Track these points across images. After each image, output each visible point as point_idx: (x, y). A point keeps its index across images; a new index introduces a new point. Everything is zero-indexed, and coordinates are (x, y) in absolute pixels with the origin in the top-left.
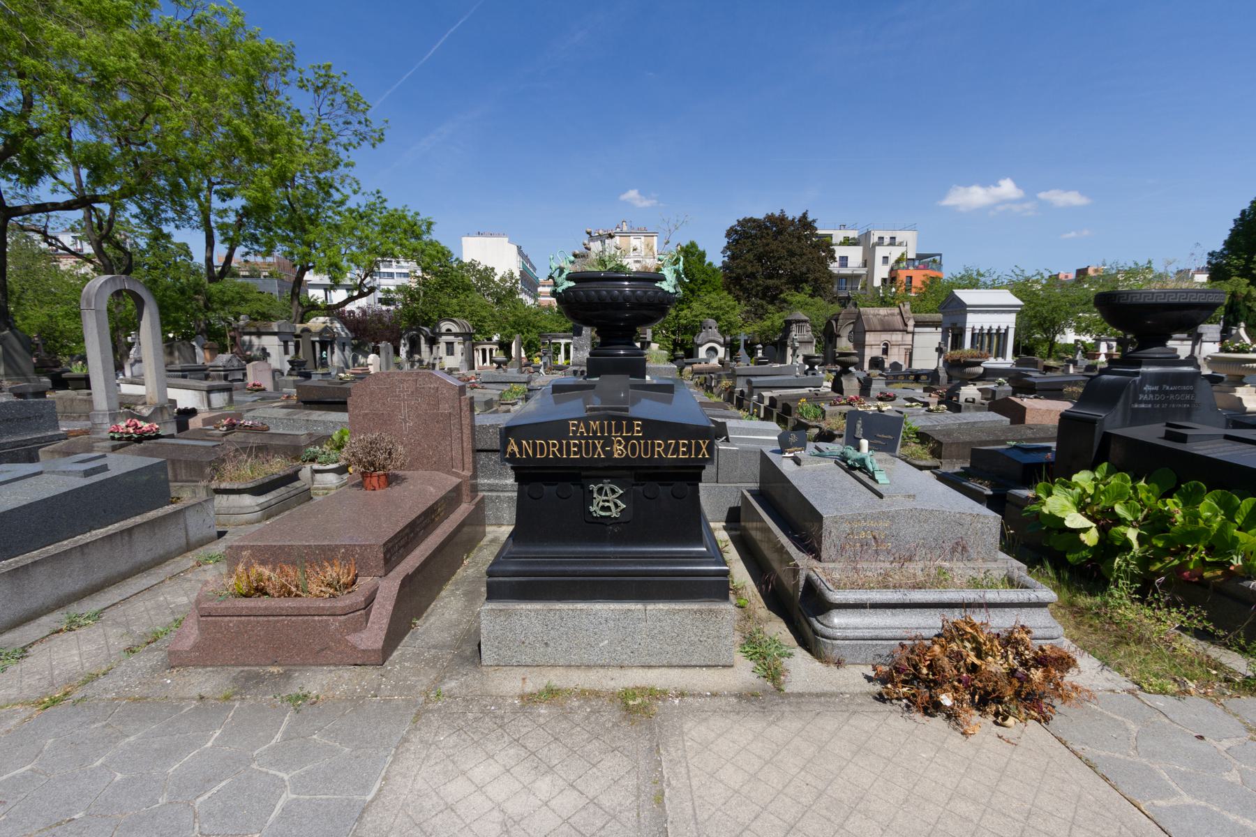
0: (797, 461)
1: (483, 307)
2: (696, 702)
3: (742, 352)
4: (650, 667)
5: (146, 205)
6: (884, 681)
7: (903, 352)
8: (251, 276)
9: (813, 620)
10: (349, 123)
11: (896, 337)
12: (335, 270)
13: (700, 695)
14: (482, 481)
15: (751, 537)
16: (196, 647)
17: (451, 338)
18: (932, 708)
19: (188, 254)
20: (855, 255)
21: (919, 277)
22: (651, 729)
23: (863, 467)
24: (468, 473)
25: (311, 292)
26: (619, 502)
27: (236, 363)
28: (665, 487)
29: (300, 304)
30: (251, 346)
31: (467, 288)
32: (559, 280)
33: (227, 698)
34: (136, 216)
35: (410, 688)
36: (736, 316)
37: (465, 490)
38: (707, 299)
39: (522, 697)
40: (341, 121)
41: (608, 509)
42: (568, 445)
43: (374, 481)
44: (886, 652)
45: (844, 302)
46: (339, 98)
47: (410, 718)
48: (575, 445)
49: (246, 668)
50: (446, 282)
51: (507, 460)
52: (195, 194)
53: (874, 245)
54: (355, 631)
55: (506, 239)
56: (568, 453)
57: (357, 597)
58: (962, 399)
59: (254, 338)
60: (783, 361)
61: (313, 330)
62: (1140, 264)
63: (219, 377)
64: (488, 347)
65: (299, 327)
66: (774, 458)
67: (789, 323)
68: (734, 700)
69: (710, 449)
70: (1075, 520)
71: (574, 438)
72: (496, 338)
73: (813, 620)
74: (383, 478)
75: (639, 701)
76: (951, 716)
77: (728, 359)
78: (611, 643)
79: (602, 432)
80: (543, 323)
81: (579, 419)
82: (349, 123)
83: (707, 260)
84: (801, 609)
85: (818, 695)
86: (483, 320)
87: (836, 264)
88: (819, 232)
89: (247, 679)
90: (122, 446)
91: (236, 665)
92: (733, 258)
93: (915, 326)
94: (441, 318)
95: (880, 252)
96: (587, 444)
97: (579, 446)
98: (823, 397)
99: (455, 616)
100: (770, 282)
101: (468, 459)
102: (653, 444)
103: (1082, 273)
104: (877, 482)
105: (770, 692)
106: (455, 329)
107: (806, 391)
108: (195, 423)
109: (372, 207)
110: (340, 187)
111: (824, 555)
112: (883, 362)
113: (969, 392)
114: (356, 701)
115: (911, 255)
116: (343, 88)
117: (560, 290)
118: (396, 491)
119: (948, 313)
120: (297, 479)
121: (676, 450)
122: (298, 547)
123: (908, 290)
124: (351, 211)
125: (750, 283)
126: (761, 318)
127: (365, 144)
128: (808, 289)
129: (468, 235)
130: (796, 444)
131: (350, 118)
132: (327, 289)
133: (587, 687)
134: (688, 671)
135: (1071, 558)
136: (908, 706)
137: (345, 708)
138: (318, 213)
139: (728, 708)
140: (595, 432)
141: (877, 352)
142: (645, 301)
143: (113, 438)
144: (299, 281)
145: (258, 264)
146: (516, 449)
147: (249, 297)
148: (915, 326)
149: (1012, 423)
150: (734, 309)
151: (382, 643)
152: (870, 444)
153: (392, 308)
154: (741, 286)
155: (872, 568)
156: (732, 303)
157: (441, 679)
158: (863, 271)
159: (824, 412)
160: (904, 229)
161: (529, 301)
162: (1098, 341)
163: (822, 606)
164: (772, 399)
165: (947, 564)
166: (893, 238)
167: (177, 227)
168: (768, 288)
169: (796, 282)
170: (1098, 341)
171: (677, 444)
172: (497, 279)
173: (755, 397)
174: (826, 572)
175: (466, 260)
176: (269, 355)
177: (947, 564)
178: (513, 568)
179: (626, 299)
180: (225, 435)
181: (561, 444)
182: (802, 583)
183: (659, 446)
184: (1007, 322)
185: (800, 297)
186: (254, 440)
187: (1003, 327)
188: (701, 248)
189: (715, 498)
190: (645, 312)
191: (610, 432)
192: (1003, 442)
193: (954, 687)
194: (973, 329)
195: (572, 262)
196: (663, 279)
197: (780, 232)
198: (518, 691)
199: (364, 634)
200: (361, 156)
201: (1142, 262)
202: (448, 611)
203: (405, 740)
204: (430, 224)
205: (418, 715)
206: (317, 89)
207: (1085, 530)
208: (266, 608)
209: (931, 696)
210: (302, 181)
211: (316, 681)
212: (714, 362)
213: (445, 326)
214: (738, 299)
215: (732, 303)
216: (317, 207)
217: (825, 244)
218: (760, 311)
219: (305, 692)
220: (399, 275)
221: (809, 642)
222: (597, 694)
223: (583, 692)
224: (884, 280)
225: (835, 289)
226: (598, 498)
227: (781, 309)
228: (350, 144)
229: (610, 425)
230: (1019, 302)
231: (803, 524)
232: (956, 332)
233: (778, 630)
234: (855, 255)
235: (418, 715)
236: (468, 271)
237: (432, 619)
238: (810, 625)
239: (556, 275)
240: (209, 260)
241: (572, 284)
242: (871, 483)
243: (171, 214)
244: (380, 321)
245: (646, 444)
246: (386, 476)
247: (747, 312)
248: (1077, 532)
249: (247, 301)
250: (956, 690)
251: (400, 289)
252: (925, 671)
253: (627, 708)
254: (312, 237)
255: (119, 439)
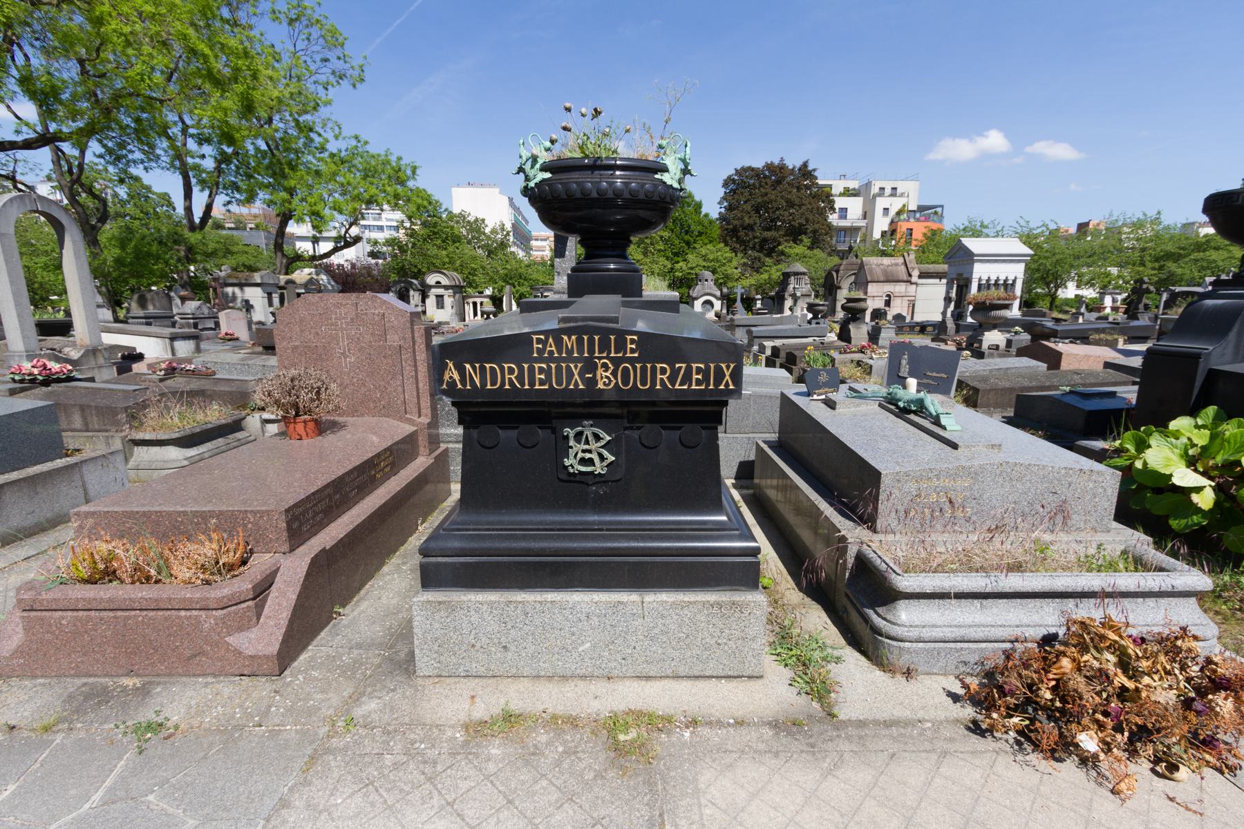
0: (831, 404)
1: (474, 258)
2: (714, 736)
3: (739, 304)
4: (648, 678)
5: (110, 144)
6: (975, 701)
7: (906, 304)
8: (236, 229)
9: (870, 612)
10: (326, 60)
11: (899, 288)
12: (318, 219)
13: (720, 724)
14: (442, 431)
15: (768, 499)
16: (19, 652)
17: (440, 291)
18: (1064, 748)
19: (170, 204)
20: (854, 207)
21: (919, 230)
22: (650, 784)
23: (921, 409)
24: (425, 420)
25: (298, 244)
26: (605, 453)
27: (206, 311)
28: (671, 429)
29: (284, 255)
30: (234, 298)
31: (457, 239)
32: (531, 173)
33: (46, 729)
34: (100, 156)
35: (311, 712)
36: (733, 269)
37: (422, 441)
38: (703, 251)
39: (466, 727)
40: (318, 58)
41: (590, 462)
42: (531, 369)
43: (300, 428)
44: (973, 658)
45: (843, 255)
46: (315, 32)
47: (300, 763)
48: (541, 370)
49: (91, 680)
50: (435, 233)
51: (444, 392)
52: (164, 132)
53: (875, 197)
54: (240, 629)
55: (497, 190)
56: (532, 384)
57: (243, 584)
58: (985, 346)
59: (237, 290)
60: (781, 311)
61: (298, 281)
62: (1149, 215)
63: (188, 325)
64: (478, 300)
65: (283, 278)
66: (801, 402)
67: (786, 276)
68: (768, 732)
69: (737, 376)
70: (1184, 477)
71: (540, 360)
72: (488, 292)
73: (870, 612)
74: (311, 425)
75: (633, 734)
76: (1087, 761)
77: (724, 311)
78: (594, 647)
79: (581, 351)
80: (535, 276)
81: (546, 333)
82: (326, 60)
83: (704, 210)
84: (857, 599)
85: (888, 724)
86: (473, 272)
87: (835, 216)
88: (820, 182)
89: (87, 697)
90: (23, 390)
91: (77, 676)
92: (730, 208)
93: (920, 277)
94: (431, 271)
95: (881, 203)
96: (559, 369)
97: (548, 372)
98: (831, 346)
99: (394, 601)
100: (768, 234)
101: (426, 402)
102: (654, 369)
103: (1082, 227)
104: (944, 428)
105: (816, 721)
106: (445, 281)
107: (810, 340)
108: (138, 367)
109: (354, 153)
110: (321, 132)
111: (880, 524)
112: (885, 313)
113: (993, 337)
114: (230, 733)
115: (913, 207)
116: (318, 21)
117: (532, 184)
118: (329, 440)
119: (954, 261)
120: (241, 429)
121: (687, 378)
122: (169, 514)
123: (908, 243)
124: (332, 155)
125: (747, 235)
126: (757, 271)
127: (344, 83)
128: (807, 240)
129: (458, 185)
130: (826, 385)
131: (328, 55)
132: (315, 240)
133: (560, 710)
134: (700, 684)
135: (1174, 524)
136: (1018, 743)
137: (211, 745)
138: (298, 158)
139: (762, 746)
140: (570, 352)
141: (879, 304)
142: (642, 196)
143: (13, 380)
144: (281, 232)
145: (242, 213)
146: (456, 376)
147: (235, 249)
148: (920, 277)
149: (1049, 369)
150: (730, 261)
151: (277, 646)
152: (919, 384)
153: (380, 261)
154: (738, 238)
155: (944, 542)
156: (728, 255)
157: (356, 698)
158: (862, 223)
159: (833, 360)
160: (906, 179)
161: (521, 254)
162: (1102, 295)
163: (886, 595)
164: (775, 349)
165: (1047, 537)
166: (894, 189)
167: (146, 169)
168: (765, 240)
169: (795, 234)
170: (1102, 295)
171: (689, 369)
172: (487, 230)
173: (756, 348)
174: (885, 546)
175: (456, 211)
176: (252, 307)
177: (1047, 537)
178: (457, 544)
179: (618, 194)
180: (161, 380)
181: (521, 370)
182: (851, 561)
183: (663, 371)
184: (1016, 272)
185: (799, 249)
186: (195, 384)
187: (1011, 278)
188: (697, 198)
189: (736, 444)
190: (642, 213)
191: (591, 351)
192: (1056, 388)
193: (1097, 721)
194: (980, 279)
195: (548, 150)
196: (665, 169)
197: (779, 182)
198: (463, 717)
199: (253, 634)
200: (339, 94)
201: (1152, 213)
202: (393, 586)
203: (284, 803)
204: (414, 169)
205: (313, 758)
206: (291, 22)
207: (1198, 490)
208: (110, 600)
209: (1061, 735)
210: (281, 125)
211: (182, 702)
212: (711, 315)
213: (431, 279)
214: (734, 250)
215: (728, 255)
216: (297, 152)
217: (826, 196)
218: (757, 264)
219: (160, 720)
220: (385, 224)
221: (866, 641)
222: (573, 722)
223: (555, 717)
224: (884, 234)
225: (834, 242)
226: (576, 447)
227: (778, 262)
228: (328, 83)
229: (591, 341)
230: (1031, 252)
231: (854, 485)
232: (962, 283)
233: (815, 621)
234: (854, 207)
235: (313, 758)
236: (458, 222)
237: (364, 605)
238: (866, 620)
239: (527, 167)
240: (189, 209)
241: (548, 175)
242: (941, 432)
243: (138, 155)
244: (369, 274)
245: (644, 369)
246: (317, 422)
247: (744, 264)
248: (1186, 492)
249: (232, 253)
250: (1101, 726)
251: (391, 242)
252: (1048, 695)
253: (619, 750)
254: (292, 183)
255: (22, 381)
